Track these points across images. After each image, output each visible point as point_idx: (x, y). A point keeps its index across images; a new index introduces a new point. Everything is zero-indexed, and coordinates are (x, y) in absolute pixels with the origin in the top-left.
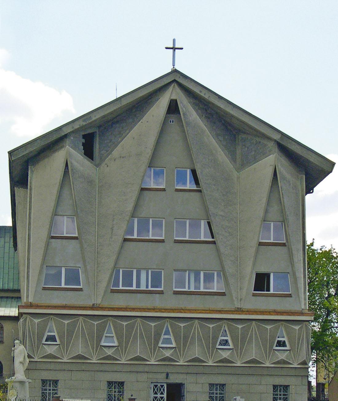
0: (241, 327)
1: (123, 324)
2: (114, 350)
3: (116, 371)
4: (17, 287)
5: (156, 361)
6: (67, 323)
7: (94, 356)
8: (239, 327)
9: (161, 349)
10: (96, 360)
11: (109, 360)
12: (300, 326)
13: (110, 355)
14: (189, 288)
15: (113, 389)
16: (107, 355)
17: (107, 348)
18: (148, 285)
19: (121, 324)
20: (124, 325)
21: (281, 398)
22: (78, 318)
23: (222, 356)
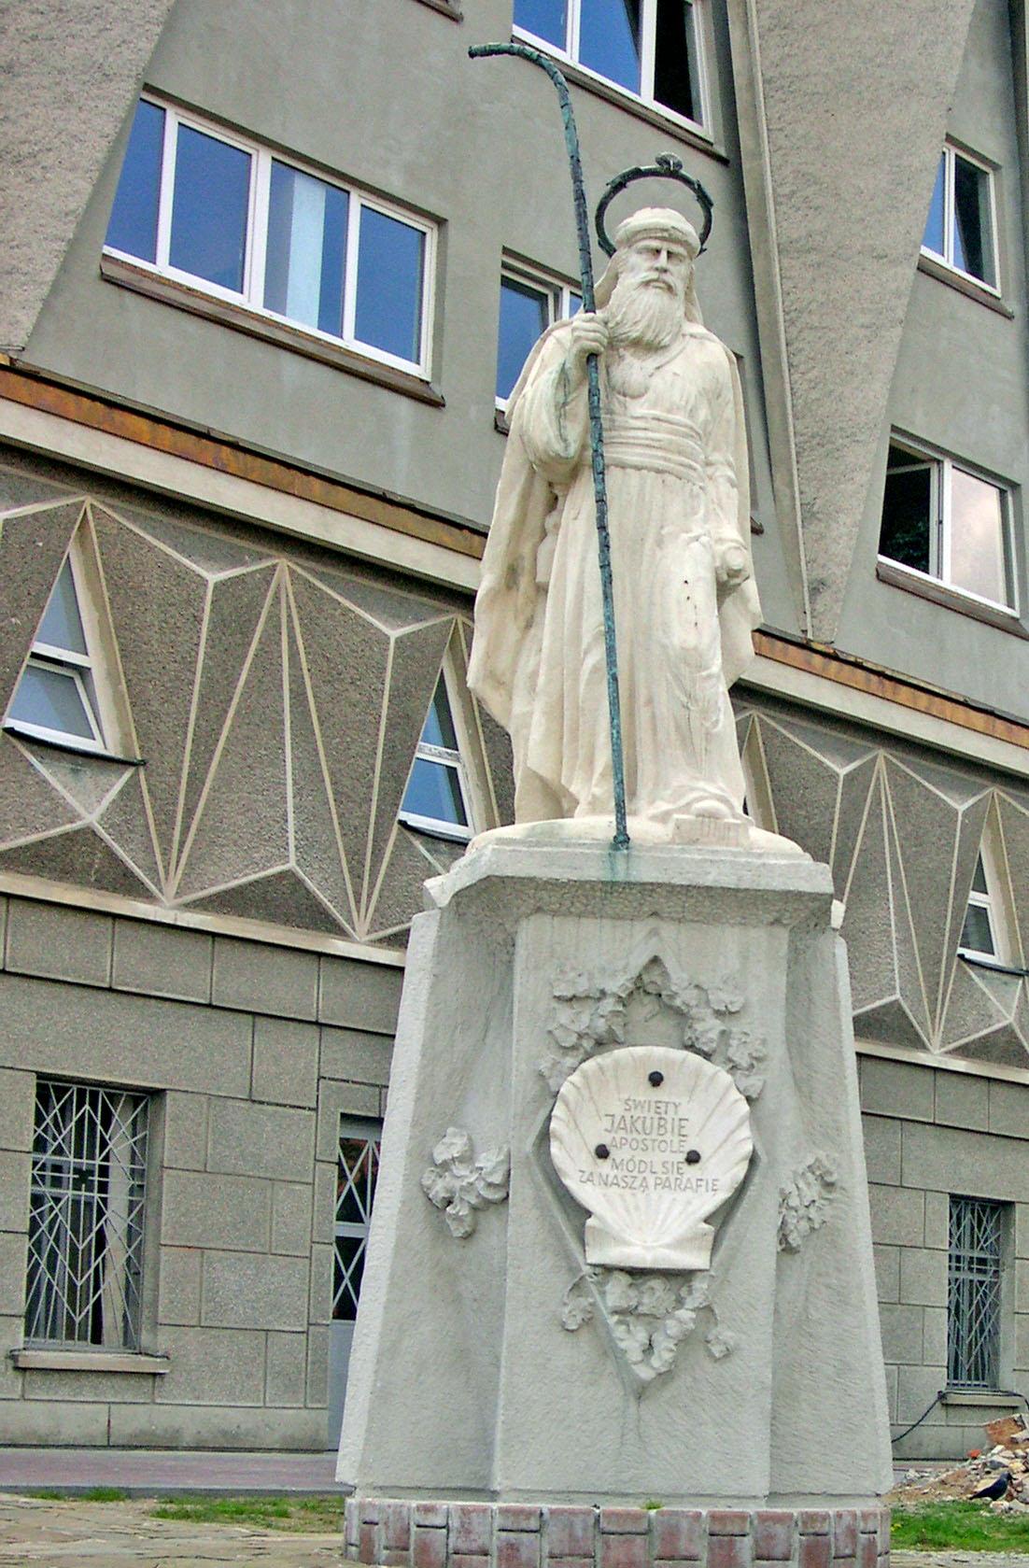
0: (966, 806)
1: (396, 642)
2: (113, 794)
3: (110, 990)
4: (632, 456)
5: (380, 940)
6: (399, 641)
7: (167, 873)
8: (204, 573)
9: (418, 844)
10: (373, 943)
11: (65, 874)
12: (972, 801)
13: (89, 832)
14: (276, 291)
15: (70, 1150)
16: (68, 827)
17: (66, 765)
18: (435, 337)
19: (182, 576)
20: (204, 583)
21: (99, 1192)
22: (269, 563)
23: (58, 810)
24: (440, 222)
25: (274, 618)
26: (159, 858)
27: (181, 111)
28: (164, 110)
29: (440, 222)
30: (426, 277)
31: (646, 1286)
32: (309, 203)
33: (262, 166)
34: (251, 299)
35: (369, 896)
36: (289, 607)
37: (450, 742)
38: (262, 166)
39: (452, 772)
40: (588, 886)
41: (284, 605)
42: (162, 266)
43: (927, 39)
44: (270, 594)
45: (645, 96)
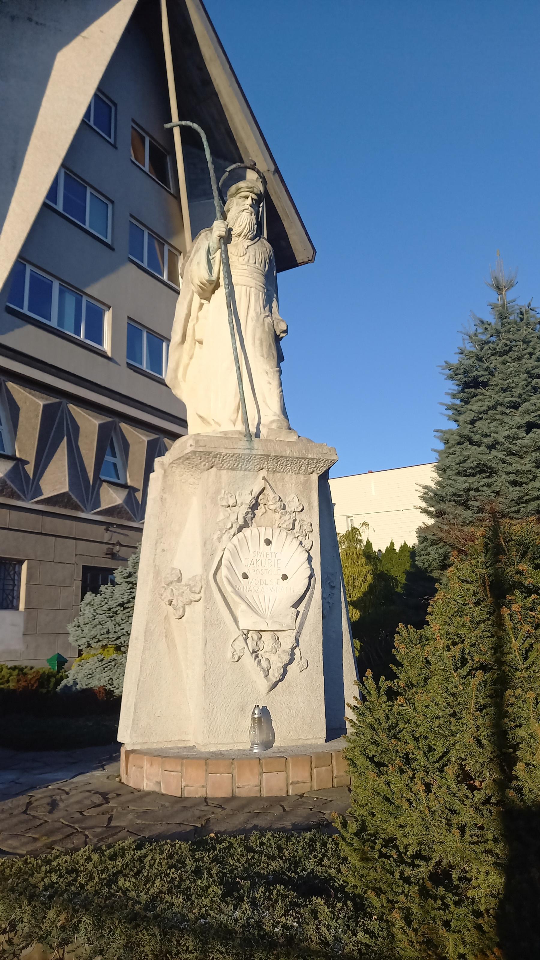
14: (61, 321)
24: (112, 202)
25: (62, 417)
26: (25, 488)
27: (31, 266)
28: (25, 265)
29: (112, 202)
30: (108, 225)
31: (219, 500)
32: (70, 300)
33: (56, 286)
34: (54, 323)
35: (91, 499)
36: (66, 415)
37: (114, 455)
38: (56, 286)
39: (115, 465)
40: (108, 696)
41: (64, 413)
42: (25, 310)
43: (63, 866)
44: (60, 410)
45: (165, 278)
